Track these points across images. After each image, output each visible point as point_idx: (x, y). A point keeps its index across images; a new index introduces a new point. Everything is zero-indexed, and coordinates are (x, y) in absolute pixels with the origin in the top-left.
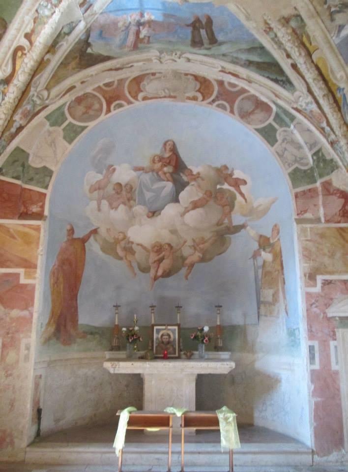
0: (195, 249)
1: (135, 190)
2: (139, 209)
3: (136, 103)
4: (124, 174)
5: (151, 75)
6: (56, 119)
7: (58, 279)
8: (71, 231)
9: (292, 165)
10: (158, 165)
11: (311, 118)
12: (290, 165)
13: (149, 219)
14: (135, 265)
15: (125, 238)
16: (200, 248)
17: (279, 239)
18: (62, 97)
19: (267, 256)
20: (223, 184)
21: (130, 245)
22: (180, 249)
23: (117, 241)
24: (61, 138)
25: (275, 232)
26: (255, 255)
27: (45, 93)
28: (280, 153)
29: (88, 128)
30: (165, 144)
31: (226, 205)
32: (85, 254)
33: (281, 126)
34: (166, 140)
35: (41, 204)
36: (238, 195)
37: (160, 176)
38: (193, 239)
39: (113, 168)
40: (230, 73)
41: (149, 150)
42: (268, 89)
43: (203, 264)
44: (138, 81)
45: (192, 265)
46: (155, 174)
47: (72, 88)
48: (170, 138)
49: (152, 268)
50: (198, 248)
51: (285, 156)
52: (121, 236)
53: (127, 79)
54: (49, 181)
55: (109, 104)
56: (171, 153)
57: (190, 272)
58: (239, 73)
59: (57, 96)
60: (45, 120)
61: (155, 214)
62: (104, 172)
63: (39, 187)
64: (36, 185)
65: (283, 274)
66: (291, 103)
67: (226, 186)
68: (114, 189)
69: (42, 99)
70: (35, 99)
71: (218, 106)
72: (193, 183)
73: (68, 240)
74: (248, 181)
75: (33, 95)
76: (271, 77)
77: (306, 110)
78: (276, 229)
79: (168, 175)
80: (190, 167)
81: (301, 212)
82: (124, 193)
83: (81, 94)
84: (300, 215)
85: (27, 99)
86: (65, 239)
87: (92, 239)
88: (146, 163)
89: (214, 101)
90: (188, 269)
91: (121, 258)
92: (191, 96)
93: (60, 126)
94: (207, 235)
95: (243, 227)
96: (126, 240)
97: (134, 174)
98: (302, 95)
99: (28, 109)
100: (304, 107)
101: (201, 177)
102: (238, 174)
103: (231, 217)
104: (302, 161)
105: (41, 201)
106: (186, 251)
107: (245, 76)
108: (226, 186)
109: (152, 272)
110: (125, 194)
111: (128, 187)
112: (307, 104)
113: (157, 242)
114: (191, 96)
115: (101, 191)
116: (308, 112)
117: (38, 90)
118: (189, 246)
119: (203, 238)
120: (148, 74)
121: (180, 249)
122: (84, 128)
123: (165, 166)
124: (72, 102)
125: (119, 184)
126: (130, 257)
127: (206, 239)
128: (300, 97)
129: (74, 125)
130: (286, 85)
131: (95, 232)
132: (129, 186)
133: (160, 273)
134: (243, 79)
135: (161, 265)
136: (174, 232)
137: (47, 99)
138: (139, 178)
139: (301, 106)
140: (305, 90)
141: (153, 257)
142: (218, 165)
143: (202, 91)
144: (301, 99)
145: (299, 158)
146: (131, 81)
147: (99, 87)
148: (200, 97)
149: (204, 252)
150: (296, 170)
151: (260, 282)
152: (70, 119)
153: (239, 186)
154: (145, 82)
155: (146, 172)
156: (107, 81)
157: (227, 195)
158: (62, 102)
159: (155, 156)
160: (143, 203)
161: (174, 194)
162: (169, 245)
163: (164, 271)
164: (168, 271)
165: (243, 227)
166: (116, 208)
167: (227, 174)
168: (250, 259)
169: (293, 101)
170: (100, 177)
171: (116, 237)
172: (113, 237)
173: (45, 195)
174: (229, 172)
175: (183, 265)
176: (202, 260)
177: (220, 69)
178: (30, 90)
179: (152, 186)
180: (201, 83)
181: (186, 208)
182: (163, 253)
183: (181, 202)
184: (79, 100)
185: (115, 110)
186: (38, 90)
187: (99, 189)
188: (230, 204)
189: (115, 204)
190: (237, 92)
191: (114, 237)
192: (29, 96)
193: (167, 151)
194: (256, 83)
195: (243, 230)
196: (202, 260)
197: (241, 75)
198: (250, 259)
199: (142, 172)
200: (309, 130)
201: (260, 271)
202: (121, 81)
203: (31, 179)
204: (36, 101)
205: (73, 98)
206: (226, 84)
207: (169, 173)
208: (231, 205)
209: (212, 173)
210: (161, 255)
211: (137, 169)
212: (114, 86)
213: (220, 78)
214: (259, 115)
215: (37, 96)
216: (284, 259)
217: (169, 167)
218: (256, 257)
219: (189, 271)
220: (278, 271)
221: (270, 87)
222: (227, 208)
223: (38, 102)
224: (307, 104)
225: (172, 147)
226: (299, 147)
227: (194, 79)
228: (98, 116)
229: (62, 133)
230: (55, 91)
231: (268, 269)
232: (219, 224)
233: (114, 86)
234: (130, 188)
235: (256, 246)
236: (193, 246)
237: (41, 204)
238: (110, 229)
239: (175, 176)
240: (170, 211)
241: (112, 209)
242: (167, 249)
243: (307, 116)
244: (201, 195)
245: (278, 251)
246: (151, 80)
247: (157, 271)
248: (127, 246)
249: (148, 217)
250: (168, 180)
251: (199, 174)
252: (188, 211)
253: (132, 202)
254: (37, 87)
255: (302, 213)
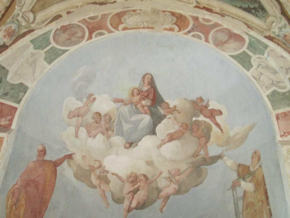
0: (171, 181)
1: (114, 121)
2: (117, 140)
3: (117, 32)
4: (104, 105)
5: (132, 11)
6: (40, 43)
7: (18, 200)
8: (43, 152)
9: (270, 88)
10: (137, 98)
11: (284, 44)
12: (268, 88)
13: (126, 150)
14: (109, 195)
15: (100, 166)
16: (176, 179)
17: (260, 166)
18: (47, 24)
19: (247, 186)
20: (199, 116)
21: (105, 174)
22: (156, 180)
23: (92, 169)
24: (42, 59)
25: (256, 160)
26: (235, 186)
27: (31, 16)
28: (257, 77)
29: (68, 52)
30: (144, 78)
31: (202, 137)
32: (56, 179)
33: (255, 54)
34: (144, 73)
35: (10, 117)
36: (214, 127)
37: (138, 109)
38: (169, 171)
39: (93, 97)
40: (204, 8)
41: (128, 83)
42: (241, 21)
43: (178, 197)
44: (119, 16)
45: (167, 197)
46: (134, 107)
47: (58, 17)
48: (148, 71)
49: (126, 199)
50: (174, 180)
51: (261, 79)
52: (97, 164)
53: (110, 14)
54: (23, 97)
55: (91, 33)
56: (149, 87)
57: (165, 204)
58: (212, 7)
59: (43, 22)
60: (30, 43)
61: (133, 145)
62: (85, 100)
63: (12, 101)
64: (8, 100)
65: (268, 204)
66: (263, 32)
67: (202, 118)
68: (93, 118)
69: (27, 21)
70: (20, 19)
71: (193, 36)
72: (169, 116)
73: (38, 160)
74: (224, 110)
75: (18, 15)
76: (244, 6)
77: (279, 36)
78: (257, 156)
79: (146, 108)
80: (166, 101)
81: (285, 133)
82: (103, 122)
83: (66, 23)
84: (284, 137)
85: (11, 17)
86: (35, 159)
87: (65, 163)
88: (125, 96)
89: (189, 32)
90: (163, 201)
91: (94, 187)
92: (168, 28)
93: (43, 49)
94: (183, 167)
95: (220, 157)
96: (101, 168)
97: (114, 105)
98: (275, 19)
99: (13, 28)
100: (277, 34)
101: (177, 111)
102: (213, 105)
103: (207, 148)
104: (279, 84)
105: (11, 115)
106: (162, 183)
107: (218, 10)
108: (202, 118)
109: (126, 203)
110: (104, 124)
111: (107, 118)
112: (280, 29)
113: (133, 172)
114: (168, 28)
115: (80, 118)
116: (281, 38)
117: (23, 10)
118: (165, 178)
119: (179, 170)
120: (129, 11)
121: (156, 180)
122: (64, 51)
123: (144, 99)
124: (57, 30)
125: (99, 114)
126: (103, 186)
127: (182, 170)
128: (273, 22)
129: (57, 49)
130: (259, 12)
131: (70, 157)
132: (108, 117)
133: (134, 204)
134: (217, 13)
135: (136, 196)
136: (150, 163)
137: (33, 23)
138: (118, 109)
139: (274, 33)
140: (278, 13)
141: (128, 188)
142: (194, 98)
143: (178, 23)
144: (274, 24)
145: (276, 82)
146: (114, 16)
147: (84, 20)
148: (176, 28)
149: (180, 184)
150: (274, 93)
151: (241, 216)
152: (53, 44)
153: (214, 117)
154: (126, 17)
155: (125, 105)
156: (92, 15)
157: (203, 127)
158: (47, 29)
159: (134, 89)
160: (121, 133)
161: (151, 126)
162: (145, 176)
163: (139, 203)
164: (142, 203)
165: (220, 157)
166: (95, 137)
167: (203, 106)
168: (228, 190)
169: (265, 30)
170: (80, 104)
171: (92, 165)
172: (88, 164)
173: (16, 109)
174: (205, 104)
175: (158, 198)
176: (178, 192)
177: (195, 4)
178: (14, 9)
179: (130, 118)
180: (177, 17)
181: (163, 140)
182: (139, 184)
183: (157, 134)
184: (64, 29)
185: (95, 37)
186: (23, 10)
187: (78, 116)
188: (205, 136)
189: (93, 132)
190: (211, 25)
191: (90, 164)
192: (14, 14)
193: (146, 85)
194: (229, 16)
195: (220, 160)
196: (178, 192)
197: (214, 9)
198: (228, 190)
199: (121, 103)
200: (282, 57)
201: (240, 203)
202: (104, 16)
203: (6, 94)
204: (21, 21)
205: (59, 27)
206: (201, 20)
207: (147, 106)
208: (207, 137)
209: (188, 106)
210: (136, 187)
211: (116, 101)
212: (98, 19)
213: (195, 15)
214: (233, 44)
215: (23, 17)
216: (268, 187)
217: (147, 100)
218: (235, 188)
219: (164, 203)
220: (262, 201)
221: (243, 18)
222: (203, 140)
223: (24, 23)
224: (280, 29)
225: (150, 81)
226: (275, 73)
227: (171, 14)
228: (80, 42)
229: (43, 55)
230: (41, 16)
231: (250, 199)
232: (195, 155)
233: (98, 19)
234: (109, 118)
235: (234, 176)
236: (169, 178)
237: (10, 117)
238: (85, 156)
239: (153, 109)
240: (147, 143)
241: (90, 137)
242: (142, 180)
243: (281, 43)
244: (177, 127)
245: (260, 179)
246: (132, 15)
247: (131, 203)
248: (102, 174)
249: (125, 148)
250: (146, 113)
251: (175, 107)
252: (165, 143)
253: (110, 132)
254: (22, 6)
255: (286, 134)
